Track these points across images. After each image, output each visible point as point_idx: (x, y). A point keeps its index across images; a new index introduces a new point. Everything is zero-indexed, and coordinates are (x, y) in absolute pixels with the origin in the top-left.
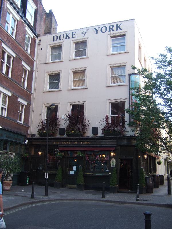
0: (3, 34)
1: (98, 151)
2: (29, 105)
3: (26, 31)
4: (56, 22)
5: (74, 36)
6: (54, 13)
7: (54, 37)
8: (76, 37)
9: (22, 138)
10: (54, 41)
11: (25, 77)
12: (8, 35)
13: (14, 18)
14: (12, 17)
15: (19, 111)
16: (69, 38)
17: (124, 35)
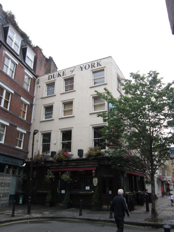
5: (64, 74)
7: (49, 76)
10: (49, 79)
14: (11, 61)
15: (18, 138)
16: (60, 76)
17: (103, 70)
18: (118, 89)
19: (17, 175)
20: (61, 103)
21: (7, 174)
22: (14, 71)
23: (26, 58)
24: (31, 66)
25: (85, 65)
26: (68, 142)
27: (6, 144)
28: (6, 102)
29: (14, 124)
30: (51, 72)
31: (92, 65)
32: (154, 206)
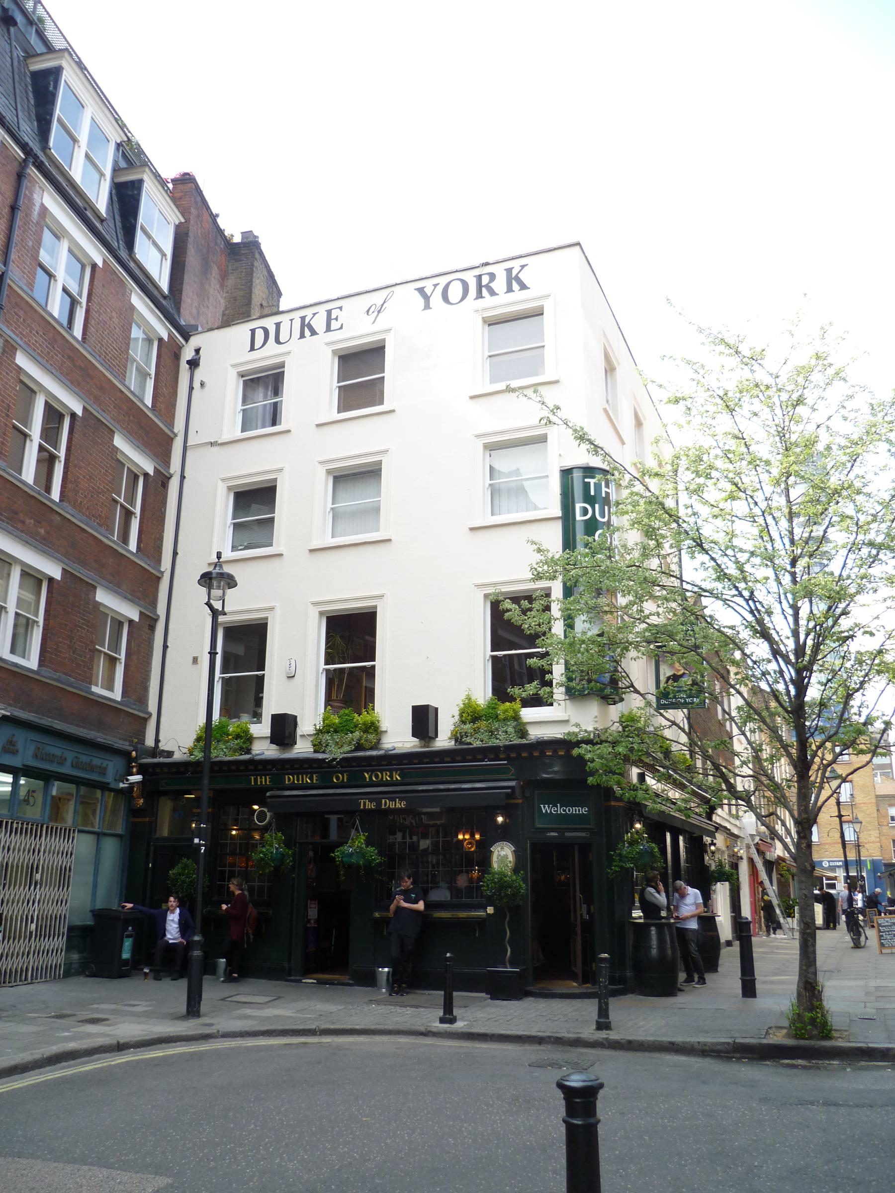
0: (21, 313)
1: (438, 810)
2: (149, 622)
3: (132, 308)
4: (275, 282)
5: (334, 325)
6: (144, 146)
7: (253, 331)
8: (341, 328)
9: (113, 766)
10: (252, 348)
11: (131, 499)
12: (46, 323)
13: (75, 252)
14: (70, 251)
15: (103, 646)
16: (313, 333)
17: (539, 313)
18: (605, 410)
19: (96, 829)
20: (321, 472)
21: (55, 825)
22: (84, 300)
23: (139, 235)
24: (161, 276)
25: (443, 281)
26: (335, 670)
27: (50, 676)
28: (47, 461)
29: (85, 574)
30: (256, 312)
31: (480, 287)
32: (812, 970)
